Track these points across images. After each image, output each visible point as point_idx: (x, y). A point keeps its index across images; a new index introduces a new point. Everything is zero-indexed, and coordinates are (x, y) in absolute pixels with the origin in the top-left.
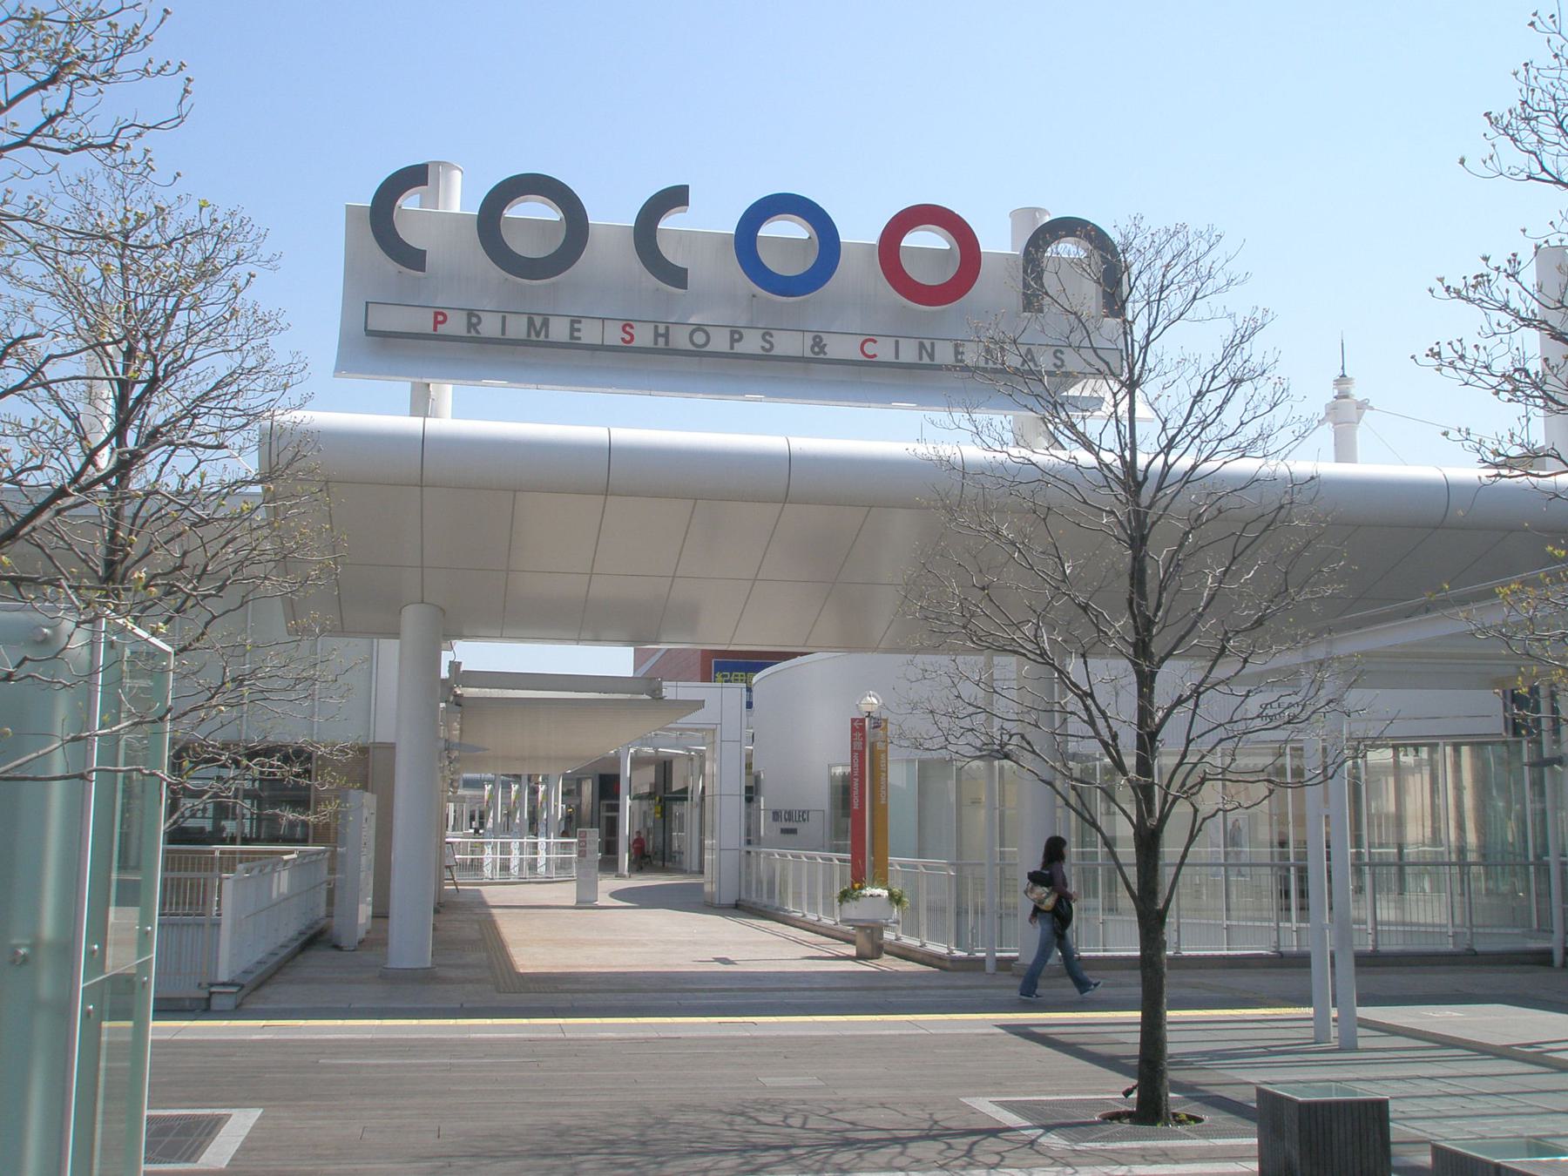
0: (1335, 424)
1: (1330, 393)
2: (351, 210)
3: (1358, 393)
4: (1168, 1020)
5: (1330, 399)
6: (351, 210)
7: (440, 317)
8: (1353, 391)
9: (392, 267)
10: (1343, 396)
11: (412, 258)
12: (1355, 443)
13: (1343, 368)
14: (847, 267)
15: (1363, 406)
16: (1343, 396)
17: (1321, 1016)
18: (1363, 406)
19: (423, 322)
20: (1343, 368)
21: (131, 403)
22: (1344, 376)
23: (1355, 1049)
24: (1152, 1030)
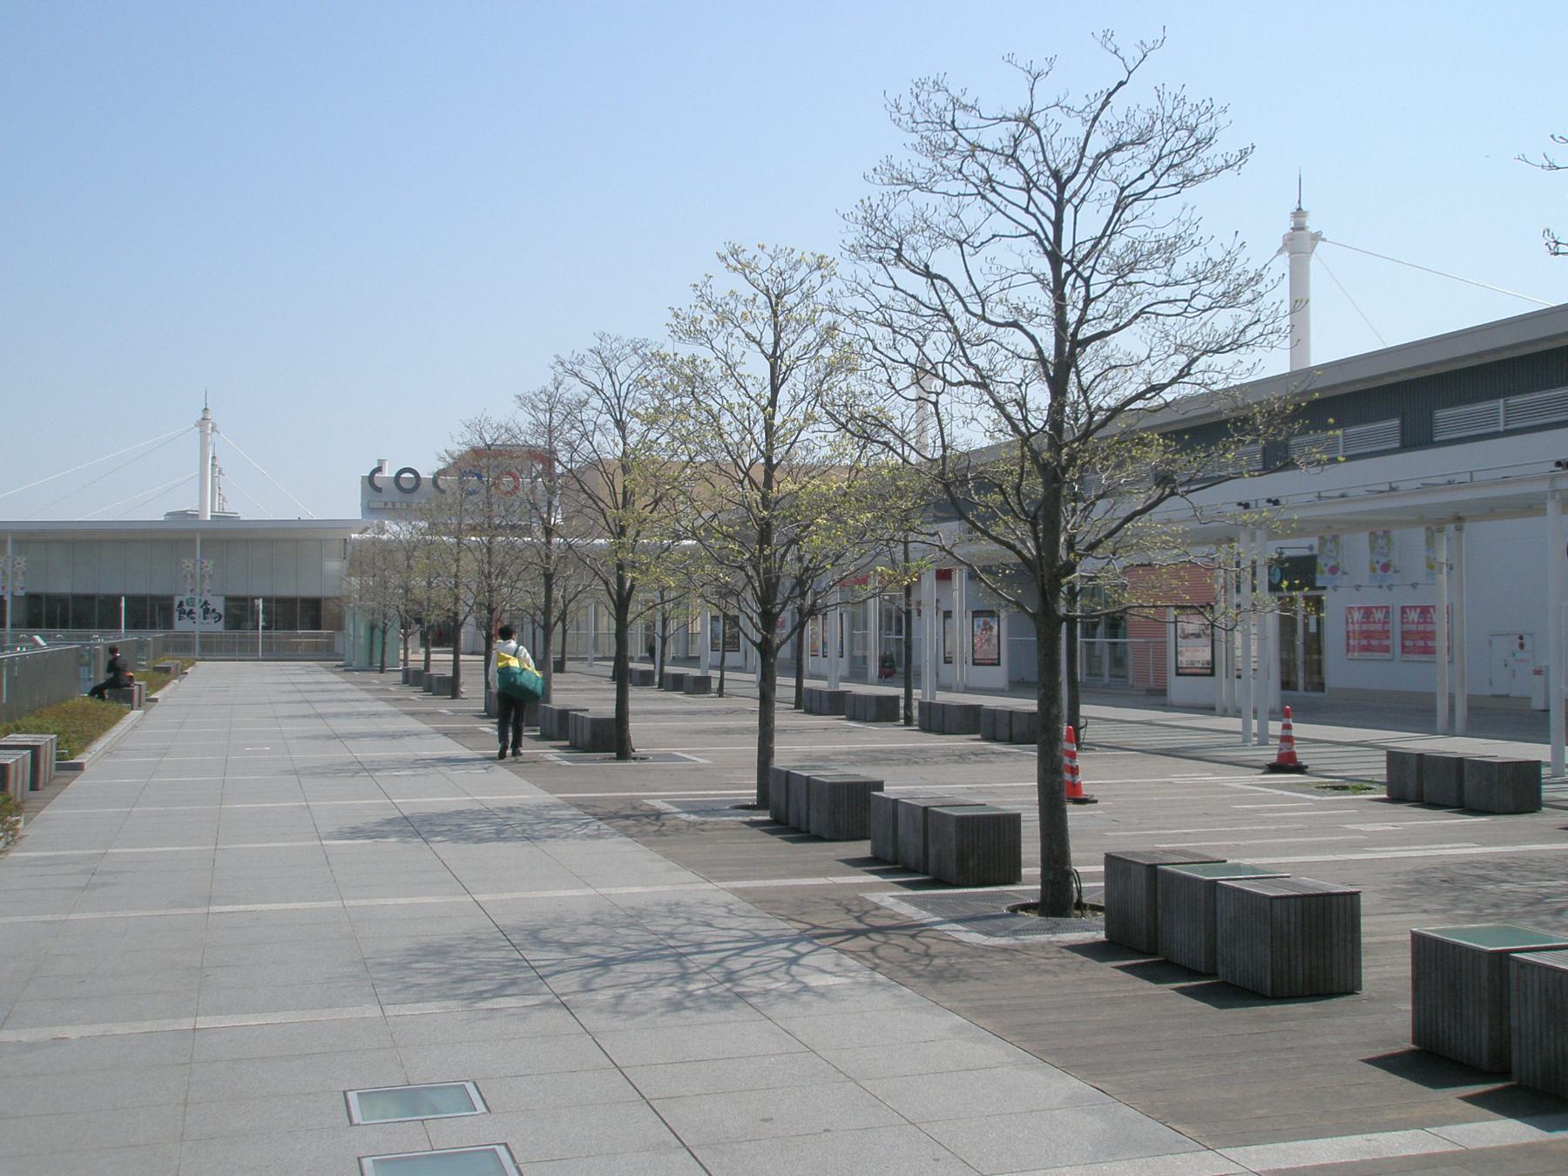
0: (1291, 254)
1: (1287, 225)
2: (363, 477)
3: (1312, 225)
4: (1384, 787)
5: (1288, 230)
6: (363, 477)
7: (386, 504)
8: (1307, 224)
9: (375, 493)
10: (1299, 228)
11: (379, 490)
12: (1308, 271)
13: (1299, 202)
14: (423, 485)
15: (1317, 237)
16: (1299, 228)
17: (1246, 725)
18: (1317, 237)
19: (382, 505)
20: (1299, 202)
21: (1063, 276)
22: (1300, 209)
23: (1267, 744)
24: (722, 676)
